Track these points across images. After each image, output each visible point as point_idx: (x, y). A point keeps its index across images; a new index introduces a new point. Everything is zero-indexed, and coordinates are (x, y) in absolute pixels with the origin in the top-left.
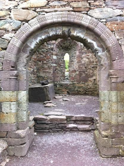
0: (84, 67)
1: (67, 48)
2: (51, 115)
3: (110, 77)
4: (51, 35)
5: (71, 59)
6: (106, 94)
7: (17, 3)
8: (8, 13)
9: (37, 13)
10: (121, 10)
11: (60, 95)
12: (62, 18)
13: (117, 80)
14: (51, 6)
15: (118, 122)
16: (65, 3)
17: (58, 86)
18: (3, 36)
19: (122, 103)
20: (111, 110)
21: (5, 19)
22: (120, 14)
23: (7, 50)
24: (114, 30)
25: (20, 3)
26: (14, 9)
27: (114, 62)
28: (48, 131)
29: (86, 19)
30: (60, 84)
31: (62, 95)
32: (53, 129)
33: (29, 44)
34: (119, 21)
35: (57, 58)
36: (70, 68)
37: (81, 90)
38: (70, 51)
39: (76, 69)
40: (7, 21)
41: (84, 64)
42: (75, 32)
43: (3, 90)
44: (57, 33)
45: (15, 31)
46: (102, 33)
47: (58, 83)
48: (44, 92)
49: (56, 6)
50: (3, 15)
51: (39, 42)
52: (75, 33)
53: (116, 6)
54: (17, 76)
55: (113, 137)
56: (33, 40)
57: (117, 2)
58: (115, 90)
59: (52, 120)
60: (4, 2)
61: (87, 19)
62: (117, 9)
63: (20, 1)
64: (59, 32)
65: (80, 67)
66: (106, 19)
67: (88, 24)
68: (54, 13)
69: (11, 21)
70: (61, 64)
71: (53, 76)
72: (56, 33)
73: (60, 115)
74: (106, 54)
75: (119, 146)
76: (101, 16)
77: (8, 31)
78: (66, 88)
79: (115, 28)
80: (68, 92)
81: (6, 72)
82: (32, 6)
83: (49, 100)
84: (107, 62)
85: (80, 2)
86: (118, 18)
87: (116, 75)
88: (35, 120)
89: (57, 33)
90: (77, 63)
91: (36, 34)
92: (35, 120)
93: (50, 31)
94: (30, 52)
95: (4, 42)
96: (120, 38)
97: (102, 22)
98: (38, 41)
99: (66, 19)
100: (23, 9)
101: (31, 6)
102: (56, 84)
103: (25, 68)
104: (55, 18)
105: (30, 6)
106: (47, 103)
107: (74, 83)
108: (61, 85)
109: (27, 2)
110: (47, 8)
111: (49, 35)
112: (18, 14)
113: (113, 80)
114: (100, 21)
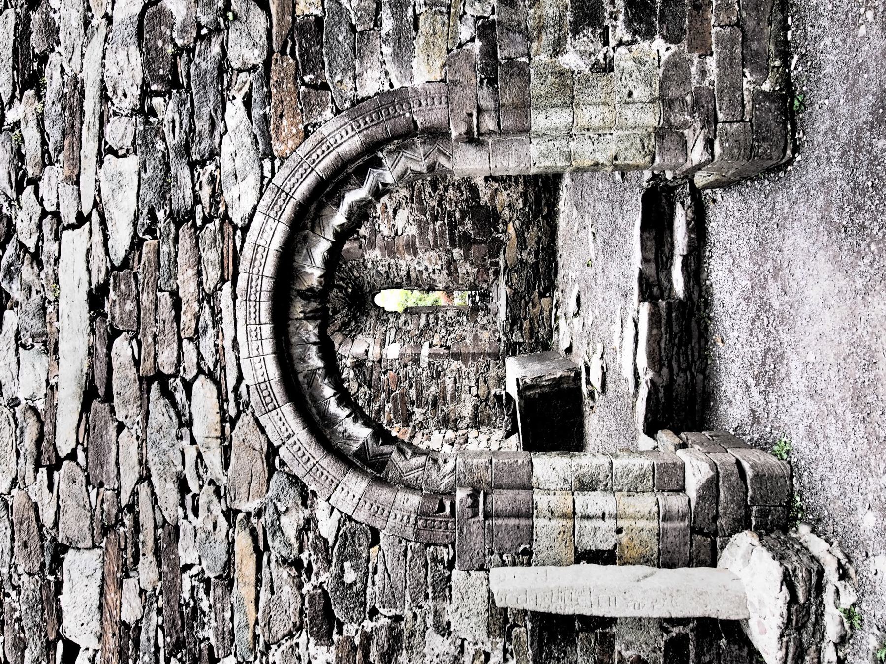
0: (431, 227)
2: (635, 365)
3: (476, 135)
4: (320, 364)
5: (397, 280)
6: (543, 147)
7: (206, 486)
8: (242, 520)
9: (243, 414)
10: (229, 104)
11: (557, 328)
13: (488, 111)
14: (216, 362)
15: (652, 102)
16: (207, 310)
17: (517, 337)
18: (326, 541)
19: (577, 87)
20: (604, 128)
21: (264, 529)
22: (243, 108)
23: (378, 527)
24: (301, 127)
25: (207, 477)
26: (229, 500)
31: (556, 318)
32: (693, 355)
33: (355, 447)
34: (268, 108)
35: (394, 341)
36: (440, 286)
37: (531, 235)
40: (273, 525)
41: (419, 223)
42: (308, 270)
44: (313, 339)
45: (310, 496)
46: (314, 172)
47: (504, 339)
48: (541, 395)
49: (216, 345)
50: (250, 541)
55: (711, 119)
56: (340, 429)
58: (527, 116)
59: (655, 360)
60: (204, 535)
62: (223, 119)
64: (311, 331)
65: (435, 242)
68: (243, 353)
69: (270, 510)
72: (314, 344)
73: (636, 325)
74: (390, 152)
75: (746, 93)
76: (252, 180)
77: (308, 521)
78: (527, 304)
80: (542, 295)
81: (461, 532)
83: (578, 375)
84: (421, 150)
85: (200, 257)
86: (257, 112)
87: (470, 115)
88: (651, 430)
89: (313, 339)
92: (651, 430)
96: (330, 105)
98: (342, 413)
100: (226, 465)
101: (219, 434)
102: (506, 344)
103: (445, 462)
104: (260, 350)
106: (588, 382)
109: (202, 450)
111: (319, 369)
113: (489, 123)
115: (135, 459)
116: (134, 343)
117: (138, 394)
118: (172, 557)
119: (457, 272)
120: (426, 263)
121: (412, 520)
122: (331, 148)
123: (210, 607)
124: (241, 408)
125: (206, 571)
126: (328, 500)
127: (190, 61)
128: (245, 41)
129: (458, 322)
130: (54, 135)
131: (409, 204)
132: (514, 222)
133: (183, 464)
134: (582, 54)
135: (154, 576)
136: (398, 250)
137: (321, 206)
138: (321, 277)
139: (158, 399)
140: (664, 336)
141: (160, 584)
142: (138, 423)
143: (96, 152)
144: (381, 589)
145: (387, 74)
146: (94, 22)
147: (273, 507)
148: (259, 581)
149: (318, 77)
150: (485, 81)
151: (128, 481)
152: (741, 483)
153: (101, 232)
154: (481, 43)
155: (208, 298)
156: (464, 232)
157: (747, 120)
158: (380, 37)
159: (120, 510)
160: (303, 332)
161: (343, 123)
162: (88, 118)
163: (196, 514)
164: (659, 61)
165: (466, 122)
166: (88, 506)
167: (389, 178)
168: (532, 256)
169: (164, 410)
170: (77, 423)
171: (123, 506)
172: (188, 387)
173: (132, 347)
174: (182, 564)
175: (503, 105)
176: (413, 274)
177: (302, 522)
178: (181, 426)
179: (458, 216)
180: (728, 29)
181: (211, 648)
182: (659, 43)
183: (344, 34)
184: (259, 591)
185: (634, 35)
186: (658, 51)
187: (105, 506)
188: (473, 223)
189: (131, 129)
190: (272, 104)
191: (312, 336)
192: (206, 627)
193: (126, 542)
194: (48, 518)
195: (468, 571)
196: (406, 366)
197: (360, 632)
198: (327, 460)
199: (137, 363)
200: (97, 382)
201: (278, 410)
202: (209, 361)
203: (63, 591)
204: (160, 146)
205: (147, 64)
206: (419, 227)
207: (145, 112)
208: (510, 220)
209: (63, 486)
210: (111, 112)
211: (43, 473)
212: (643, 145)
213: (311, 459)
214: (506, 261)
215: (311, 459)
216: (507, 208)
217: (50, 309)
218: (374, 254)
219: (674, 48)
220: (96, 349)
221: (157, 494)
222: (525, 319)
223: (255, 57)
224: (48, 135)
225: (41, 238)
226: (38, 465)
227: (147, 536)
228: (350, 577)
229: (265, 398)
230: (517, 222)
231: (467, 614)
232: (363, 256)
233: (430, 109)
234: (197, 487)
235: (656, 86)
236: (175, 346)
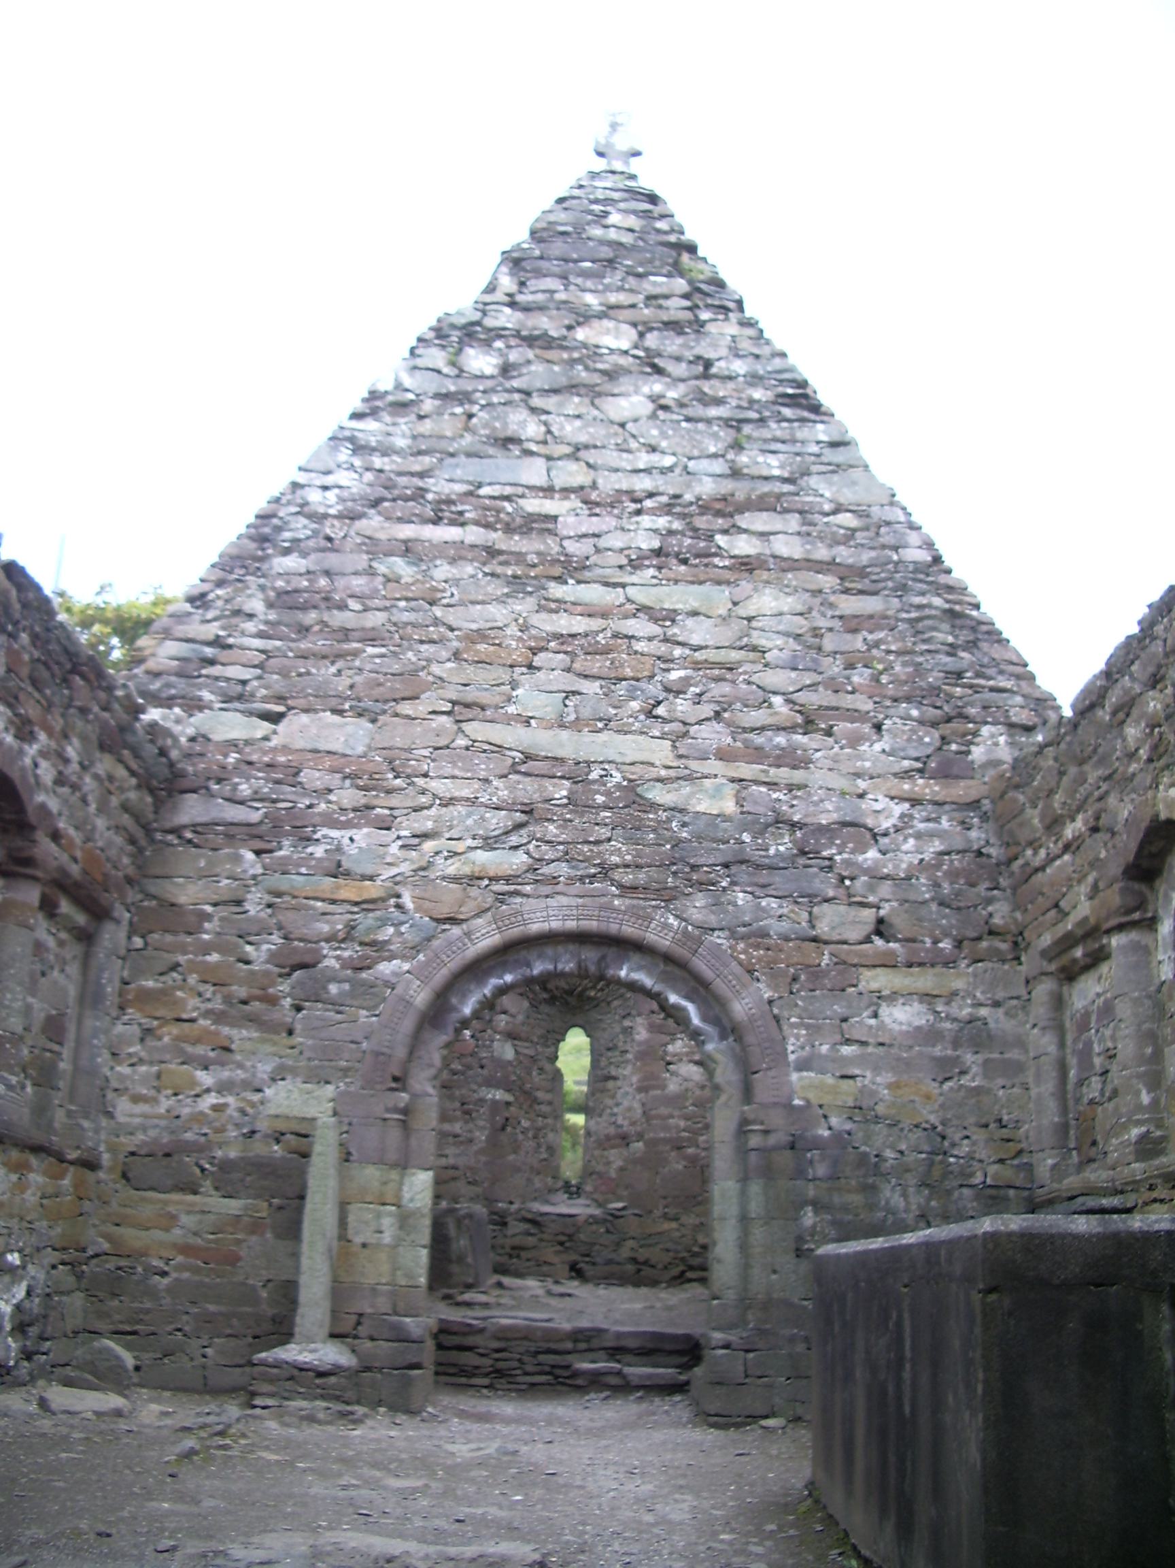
0: (676, 1113)
1: (581, 995)
4: (535, 972)
5: (603, 1062)
12: (578, 919)
16: (593, 871)
17: (516, 1227)
18: (369, 968)
27: (756, 1076)
28: (486, 1381)
29: (663, 928)
30: (530, 1216)
35: (517, 1052)
37: (655, 1254)
38: (595, 1015)
39: (633, 1124)
44: (560, 966)
53: (764, 886)
54: (406, 1111)
66: (729, 929)
67: (668, 943)
69: (403, 917)
70: (540, 1095)
74: (732, 1049)
78: (561, 1244)
87: (762, 1123)
90: (640, 1089)
98: (487, 991)
99: (595, 923)
108: (535, 1222)
112: (427, 895)
113: (754, 1141)
115: (457, 794)
116: (565, 801)
120: (626, 1103)
128: (837, 919)
129: (539, 1145)
130: (759, 740)
132: (678, 1230)
133: (450, 839)
135: (346, 803)
146: (859, 781)
148: (333, 902)
151: (438, 786)
152: (404, 1364)
159: (408, 777)
160: (568, 956)
162: (772, 771)
167: (710, 1047)
178: (486, 839)
179: (690, 1151)
181: (270, 851)
187: (413, 762)
189: (761, 810)
194: (406, 708)
205: (822, 830)
207: (780, 821)
211: (447, 707)
216: (697, 1221)
218: (642, 1034)
225: (665, 721)
226: (454, 703)
227: (383, 799)
228: (333, 989)
230: (677, 1234)
232: (639, 1015)
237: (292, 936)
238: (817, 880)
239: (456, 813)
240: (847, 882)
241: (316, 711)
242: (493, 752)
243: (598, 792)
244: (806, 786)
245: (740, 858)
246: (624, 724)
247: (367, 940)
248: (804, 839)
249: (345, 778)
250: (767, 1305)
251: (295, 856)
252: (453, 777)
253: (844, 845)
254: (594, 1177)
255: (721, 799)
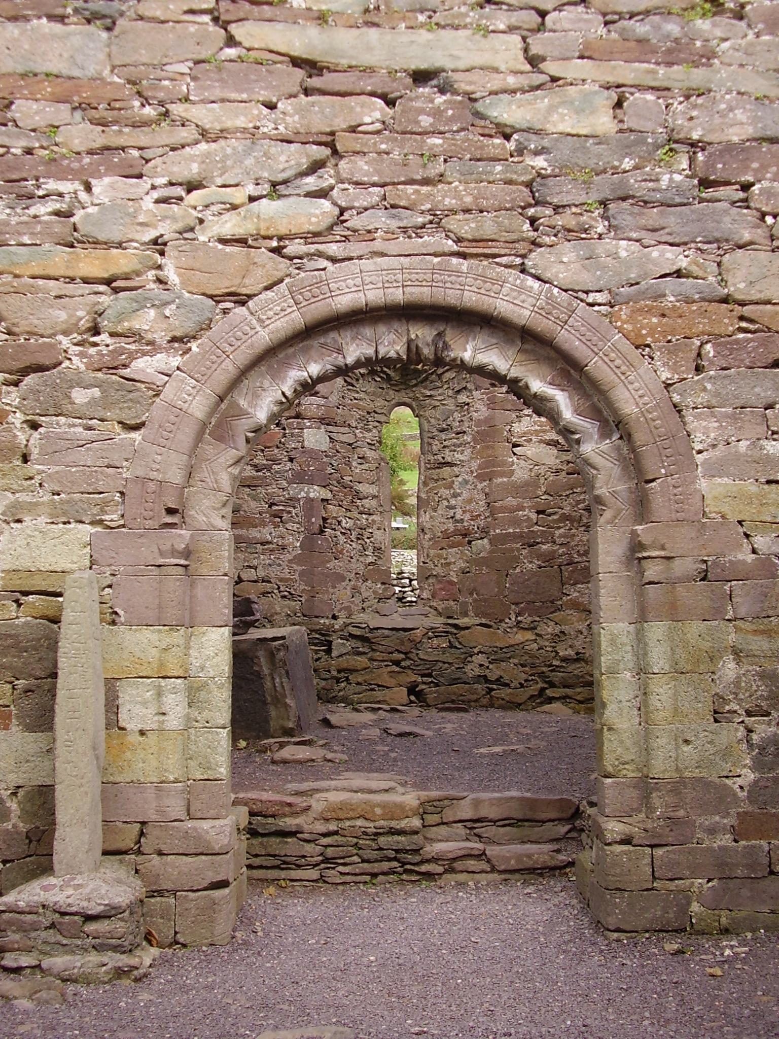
6: (624, 639)
7: (195, 213)
14: (355, 231)
15: (677, 769)
16: (420, 220)
17: (340, 645)
18: (125, 366)
22: (675, 268)
24: (649, 340)
25: (208, 215)
28: (314, 874)
29: (520, 293)
33: (243, 403)
34: (672, 299)
37: (510, 670)
41: (533, 483)
42: (469, 347)
43: (122, 619)
44: (382, 351)
46: (593, 355)
48: (259, 675)
51: (295, 391)
52: (466, 350)
53: (654, 230)
54: (187, 553)
55: (656, 841)
56: (266, 384)
57: (661, 212)
61: (522, 289)
62: (660, 243)
63: (207, 206)
65: (503, 509)
66: (610, 291)
69: (166, 296)
71: (302, 574)
72: (376, 352)
73: (386, 791)
74: (618, 449)
76: (586, 279)
78: (397, 663)
79: (651, 333)
80: (412, 690)
82: (268, 229)
87: (663, 548)
91: (281, 356)
93: (348, 339)
94: (248, 441)
95: (131, 396)
96: (676, 376)
97: (592, 305)
100: (223, 241)
101: (263, 233)
105: (258, 229)
107: (456, 626)
109: (242, 210)
110: (338, 238)
112: (197, 265)
114: (582, 301)
115: (229, 124)
116: (378, 126)
117: (313, 131)
118: (102, 168)
119: (451, 547)
120: (465, 495)
121: (154, 475)
122: (623, 378)
123: (35, 217)
124: (295, 261)
125: (82, 212)
126: (178, 368)
127: (733, 203)
130: (641, 28)
131: (565, 467)
134: (737, 683)
136: (488, 447)
137: (549, 361)
138: (462, 361)
139: (308, 156)
140: (371, 825)
141: (64, 151)
142: (277, 129)
143: (621, 81)
144: (65, 436)
145: (714, 446)
147: (169, 299)
149: (712, 363)
150: (704, 567)
151: (202, 114)
152: (205, 884)
153: (519, 86)
154: (749, 561)
155: (436, 220)
156: (516, 559)
157: (655, 885)
158: (759, 439)
159: (161, 103)
161: (654, 392)
162: (662, 70)
163: (158, 201)
164: (727, 777)
165: (653, 542)
166: (165, 60)
167: (587, 449)
168: (478, 671)
169: (293, 162)
170: (275, 49)
171: (167, 106)
172: (323, 194)
173: (372, 123)
174: (93, 182)
175: (674, 588)
176: (446, 471)
177: (149, 336)
178: (274, 185)
180: (766, 861)
182: (749, 776)
183: (762, 395)
184: (57, 280)
185: (759, 747)
186: (739, 776)
187: (166, 83)
188: (534, 574)
189: (648, 126)
190: (678, 304)
191: (387, 349)
192: (8, 211)
193: (120, 109)
195: (90, 544)
196: (291, 460)
197: (8, 408)
198: (231, 368)
199: (353, 129)
200: (327, 76)
201: (295, 308)
202: (355, 221)
203: (52, 24)
204: (627, 164)
205: (729, 148)
206: (526, 484)
208: (537, 635)
209: (192, 29)
210: (671, 101)
212: (627, 763)
213: (232, 349)
214: (467, 628)
215: (232, 349)
216: (557, 629)
217: (422, 18)
218: (481, 411)
219: (743, 795)
220: (370, 77)
221: (184, 150)
222: (372, 659)
223: (738, 286)
224: (642, 20)
227: (127, 136)
228: (80, 396)
229: (310, 291)
231: (33, 544)
233: (670, 499)
234: (193, 203)
235: (697, 773)
236: (375, 179)
237: (16, 330)
238: (727, 219)
239: (229, 151)
240: (769, 220)
241: (26, 19)
242: (275, 63)
243: (422, 111)
244: (710, 91)
245: (620, 193)
246: (455, 16)
247: (119, 329)
248: (710, 164)
249: (74, 109)
250: (678, 785)
251: (14, 220)
252: (223, 100)
253: (764, 168)
254: (431, 580)
255: (592, 113)
